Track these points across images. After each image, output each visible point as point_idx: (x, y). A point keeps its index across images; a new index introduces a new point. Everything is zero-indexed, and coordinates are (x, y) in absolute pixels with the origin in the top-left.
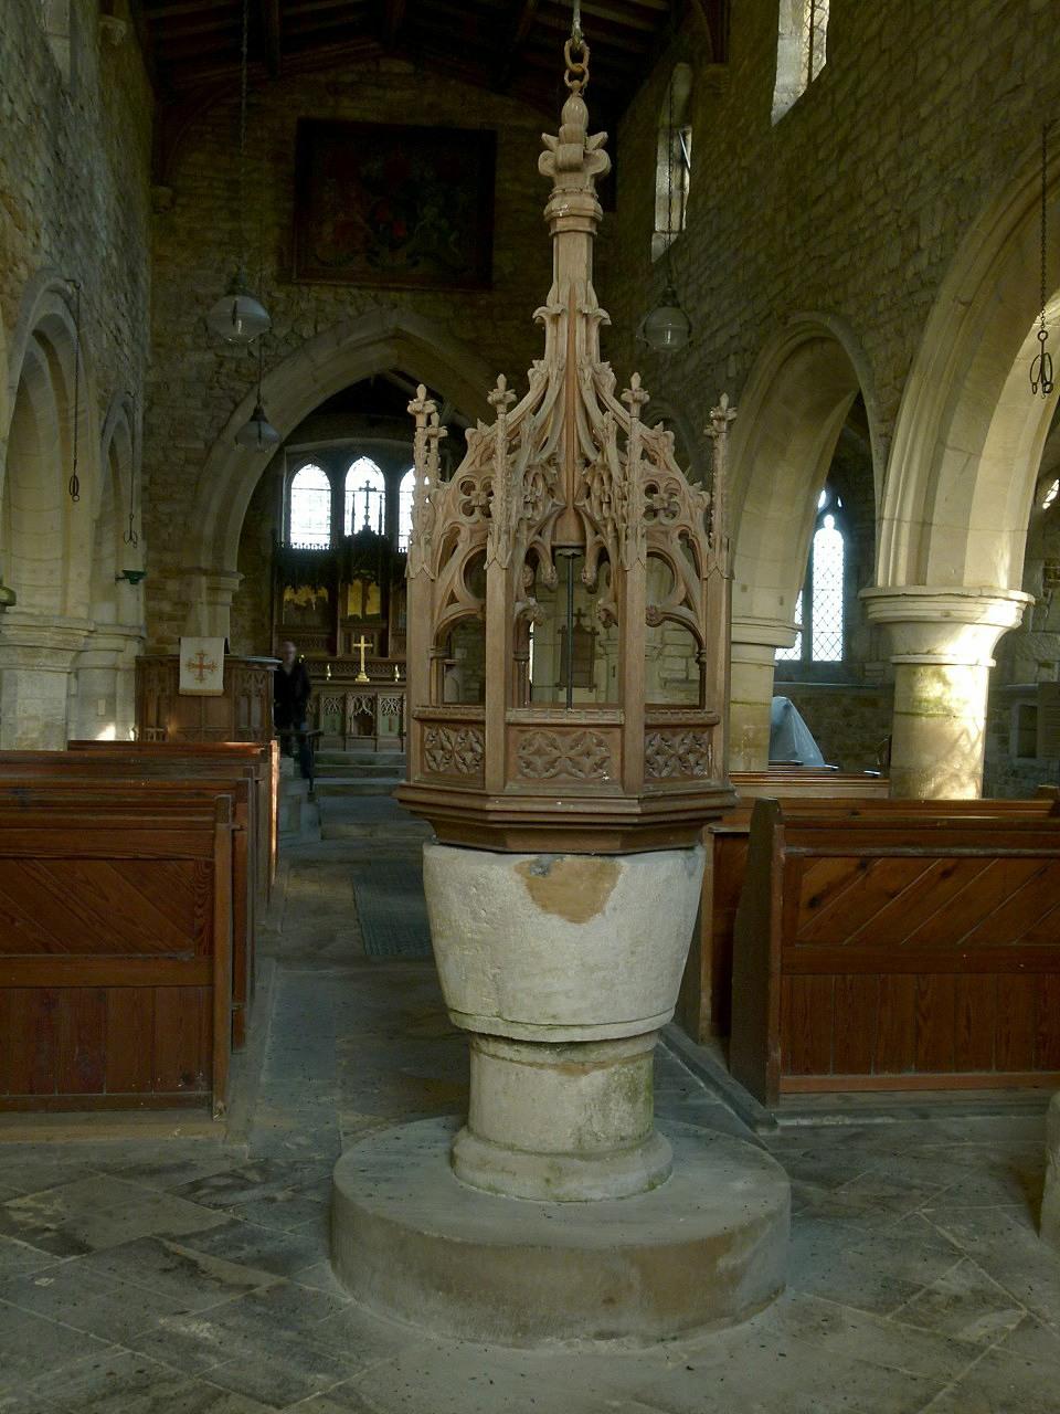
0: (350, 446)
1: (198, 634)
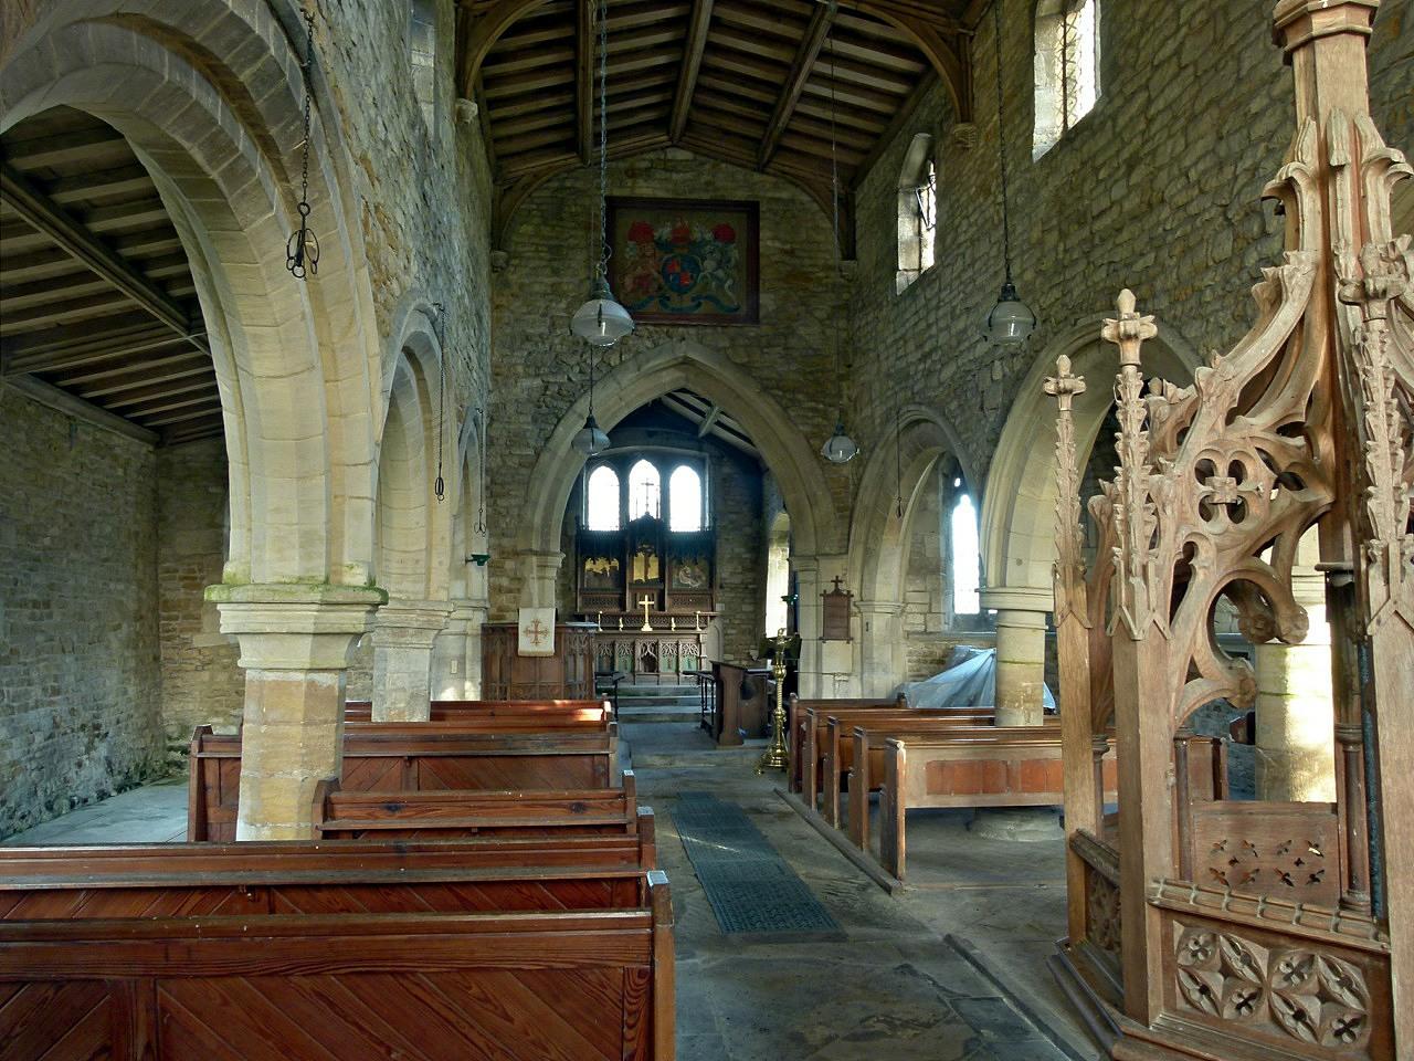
0: (632, 453)
1: (529, 605)
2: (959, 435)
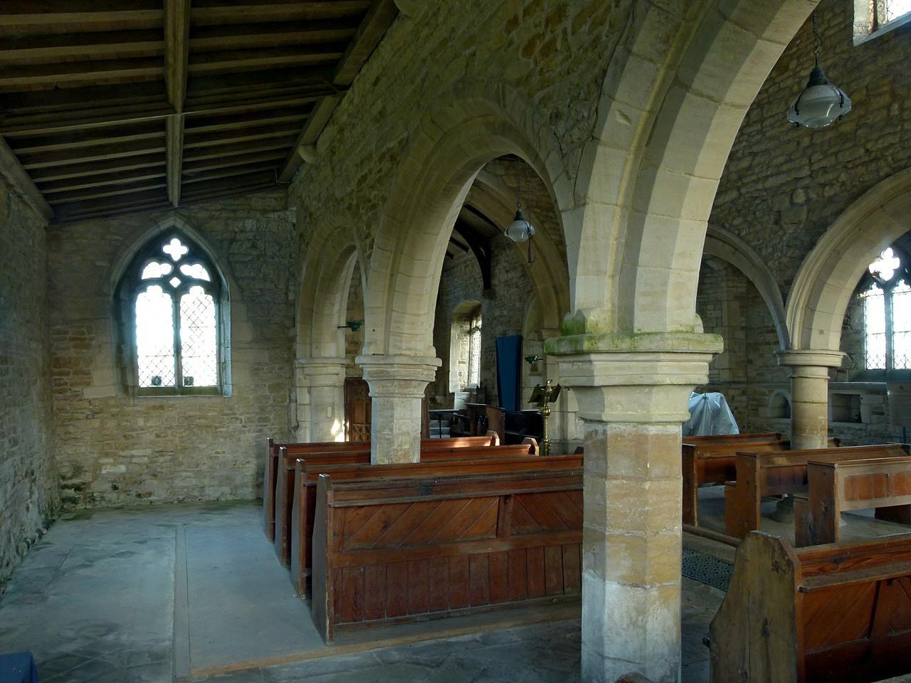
2: (748, 243)
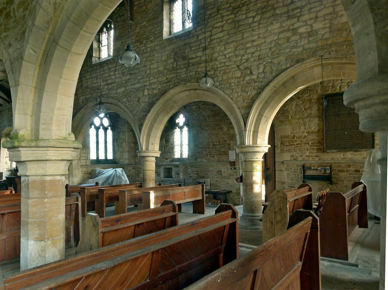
2: (128, 109)
